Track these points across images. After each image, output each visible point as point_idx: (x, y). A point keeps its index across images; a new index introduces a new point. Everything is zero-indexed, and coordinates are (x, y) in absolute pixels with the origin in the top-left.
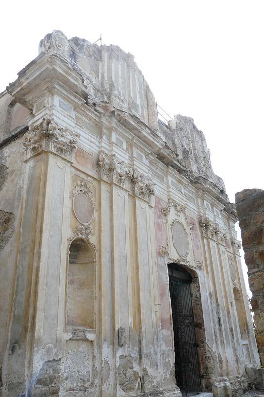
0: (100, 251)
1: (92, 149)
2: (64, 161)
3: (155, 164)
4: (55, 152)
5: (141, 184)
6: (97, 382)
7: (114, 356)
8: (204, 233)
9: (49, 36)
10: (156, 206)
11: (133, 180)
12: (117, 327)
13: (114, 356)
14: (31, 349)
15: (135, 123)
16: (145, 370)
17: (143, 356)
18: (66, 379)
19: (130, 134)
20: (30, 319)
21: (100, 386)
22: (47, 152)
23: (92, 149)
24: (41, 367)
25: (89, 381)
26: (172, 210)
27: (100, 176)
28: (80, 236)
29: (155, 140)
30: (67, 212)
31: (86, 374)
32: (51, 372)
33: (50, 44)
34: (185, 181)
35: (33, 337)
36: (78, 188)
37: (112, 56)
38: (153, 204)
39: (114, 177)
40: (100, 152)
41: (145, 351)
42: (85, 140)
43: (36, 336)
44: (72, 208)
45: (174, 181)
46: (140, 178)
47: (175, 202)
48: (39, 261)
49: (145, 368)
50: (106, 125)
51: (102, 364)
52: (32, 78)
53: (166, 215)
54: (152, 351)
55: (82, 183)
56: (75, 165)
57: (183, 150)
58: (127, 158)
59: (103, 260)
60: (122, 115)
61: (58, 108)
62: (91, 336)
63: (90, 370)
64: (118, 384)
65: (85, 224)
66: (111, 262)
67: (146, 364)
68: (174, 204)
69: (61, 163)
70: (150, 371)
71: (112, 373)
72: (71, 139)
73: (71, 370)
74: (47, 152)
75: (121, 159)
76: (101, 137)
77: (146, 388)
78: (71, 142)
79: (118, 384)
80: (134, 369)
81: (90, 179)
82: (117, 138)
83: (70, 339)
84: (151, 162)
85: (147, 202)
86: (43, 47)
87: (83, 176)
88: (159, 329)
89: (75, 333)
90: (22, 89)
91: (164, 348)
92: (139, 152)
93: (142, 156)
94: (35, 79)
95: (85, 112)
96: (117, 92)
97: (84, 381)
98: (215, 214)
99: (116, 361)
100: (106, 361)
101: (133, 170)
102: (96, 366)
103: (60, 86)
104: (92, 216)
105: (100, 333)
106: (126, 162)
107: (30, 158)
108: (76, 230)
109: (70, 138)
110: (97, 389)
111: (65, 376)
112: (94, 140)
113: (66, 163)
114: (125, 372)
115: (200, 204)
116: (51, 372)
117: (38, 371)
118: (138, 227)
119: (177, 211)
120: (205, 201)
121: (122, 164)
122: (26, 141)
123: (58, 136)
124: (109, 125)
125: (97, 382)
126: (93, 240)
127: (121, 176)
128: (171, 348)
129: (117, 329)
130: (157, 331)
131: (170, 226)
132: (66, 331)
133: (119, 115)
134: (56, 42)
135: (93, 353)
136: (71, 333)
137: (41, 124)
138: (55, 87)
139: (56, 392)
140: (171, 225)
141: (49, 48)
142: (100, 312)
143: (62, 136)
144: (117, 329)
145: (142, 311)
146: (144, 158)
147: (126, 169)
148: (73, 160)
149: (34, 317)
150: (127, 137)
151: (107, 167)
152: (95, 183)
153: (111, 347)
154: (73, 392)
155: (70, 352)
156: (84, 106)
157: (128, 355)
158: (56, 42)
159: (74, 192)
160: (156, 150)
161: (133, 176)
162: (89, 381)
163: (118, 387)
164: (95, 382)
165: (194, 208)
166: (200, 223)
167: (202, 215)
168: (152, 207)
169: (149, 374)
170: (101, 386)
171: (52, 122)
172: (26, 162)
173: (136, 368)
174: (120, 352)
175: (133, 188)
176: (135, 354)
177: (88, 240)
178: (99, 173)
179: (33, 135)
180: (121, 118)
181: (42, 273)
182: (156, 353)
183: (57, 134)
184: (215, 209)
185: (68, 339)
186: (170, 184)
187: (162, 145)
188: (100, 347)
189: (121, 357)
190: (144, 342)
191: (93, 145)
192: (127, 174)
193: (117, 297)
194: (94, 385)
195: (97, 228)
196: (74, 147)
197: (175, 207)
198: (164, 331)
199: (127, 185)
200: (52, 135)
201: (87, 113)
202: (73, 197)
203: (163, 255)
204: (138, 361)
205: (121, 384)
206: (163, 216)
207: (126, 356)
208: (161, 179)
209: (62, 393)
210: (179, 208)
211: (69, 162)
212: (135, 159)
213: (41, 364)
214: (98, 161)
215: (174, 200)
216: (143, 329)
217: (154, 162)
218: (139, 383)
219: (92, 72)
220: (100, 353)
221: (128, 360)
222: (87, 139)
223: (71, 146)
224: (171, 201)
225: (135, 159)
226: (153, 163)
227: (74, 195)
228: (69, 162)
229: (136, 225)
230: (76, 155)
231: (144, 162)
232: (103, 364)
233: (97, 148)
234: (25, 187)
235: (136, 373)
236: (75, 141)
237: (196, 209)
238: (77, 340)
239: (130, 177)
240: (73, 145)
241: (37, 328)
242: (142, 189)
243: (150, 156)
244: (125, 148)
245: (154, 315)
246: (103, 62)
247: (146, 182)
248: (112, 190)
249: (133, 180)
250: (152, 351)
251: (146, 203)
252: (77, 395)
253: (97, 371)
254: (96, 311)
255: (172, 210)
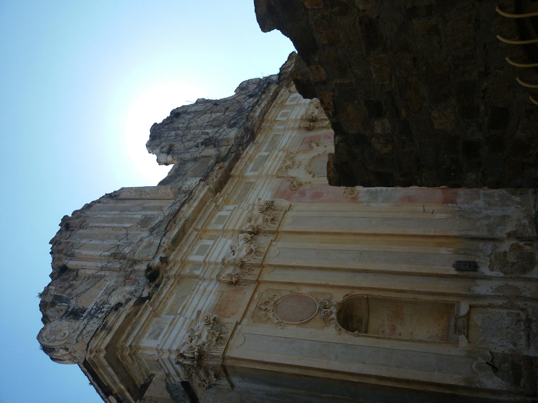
0: (353, 288)
1: (214, 291)
2: (235, 334)
3: (228, 195)
4: (224, 347)
5: (260, 221)
6: (520, 304)
7: (490, 278)
8: (323, 125)
9: (47, 349)
10: (288, 199)
11: (255, 233)
12: (453, 271)
13: (490, 278)
14: (478, 390)
15: (175, 227)
16: (510, 235)
17: (491, 236)
18: (515, 344)
19: (191, 234)
20: (441, 390)
21: (526, 300)
22: (224, 358)
23: (214, 291)
24: (500, 379)
25: (519, 314)
26: (292, 173)
27: (251, 282)
28: (334, 316)
29: (197, 197)
30: (303, 332)
31: (510, 318)
32: (506, 365)
33: (61, 348)
34: (250, 150)
35: (463, 388)
36: (270, 315)
37: (69, 253)
38: (285, 203)
39: (253, 262)
40: (219, 280)
41: (485, 233)
42: (202, 302)
43: (462, 384)
44: (298, 325)
45: (251, 166)
46: (253, 223)
47: (282, 168)
48: (369, 376)
49: (506, 234)
50: (179, 269)
51: (499, 296)
52: (116, 378)
53: (300, 184)
54: (485, 222)
55: (263, 308)
56: (238, 317)
57: (204, 146)
58: (224, 240)
59: (364, 284)
60: (165, 246)
61: (159, 341)
62: (464, 309)
63: (505, 311)
64: (525, 276)
65: (318, 307)
66: (367, 273)
67: (500, 233)
68: (284, 169)
69: (236, 341)
70: (510, 228)
71: (510, 283)
72: (203, 323)
73: (504, 338)
74: (224, 358)
75: (227, 248)
76: (197, 277)
77: (532, 235)
78: (208, 323)
79: (525, 276)
80: (508, 250)
81: (256, 297)
82: (197, 254)
83: (467, 337)
84: (227, 202)
85: (284, 214)
86: (65, 358)
87: (253, 307)
88: (456, 209)
89: (459, 330)
90: (128, 390)
91: (480, 203)
92: (214, 221)
93: (220, 216)
94: (117, 374)
95: (162, 300)
96: (126, 249)
97: (519, 321)
98: (294, 103)
99: (496, 277)
100: (495, 290)
101: (242, 232)
102: (501, 303)
103: (127, 338)
104: (306, 297)
105: (459, 295)
106: (230, 242)
107: (229, 381)
108: (326, 320)
109: (201, 324)
110: (529, 304)
111: (511, 346)
112: (202, 288)
113: (237, 331)
114: (510, 265)
115: (282, 127)
116: (506, 365)
117: (504, 382)
118: (319, 230)
119: (293, 165)
120: (278, 119)
121: (234, 249)
122: (204, 386)
123: (200, 343)
124: (179, 265)
125: (520, 304)
126: (339, 297)
127: (252, 251)
128: (482, 191)
129: (456, 273)
130: (459, 211)
131: (316, 178)
132: (456, 343)
133: (165, 251)
134: (59, 340)
135: (485, 307)
136: (460, 337)
137: (183, 365)
138: (130, 346)
139: (530, 360)
140: (313, 176)
141: (67, 349)
142: (433, 294)
143: (200, 337)
144: (456, 273)
145: (432, 233)
146: (222, 213)
147: (241, 243)
148: (233, 320)
149: (439, 385)
150: (195, 238)
151: (238, 270)
152: (262, 288)
153: (478, 282)
154: (531, 337)
155: (482, 338)
156: (154, 301)
157: (489, 259)
158: (59, 340)
159: (276, 321)
160: (210, 194)
161: (250, 233)
162: (519, 314)
163: (528, 275)
164: (521, 306)
165: (287, 138)
166: (309, 129)
167: (297, 125)
168: (291, 206)
169: (515, 229)
170: (526, 299)
171: (182, 351)
172: (232, 386)
173: (505, 247)
174: (485, 270)
175: (266, 233)
176: (489, 247)
177: (339, 304)
178: (248, 282)
179: (197, 377)
180: (169, 249)
181: (384, 373)
182: (488, 217)
183: (198, 344)
184: (288, 103)
185: (466, 340)
186: (257, 173)
187: (204, 186)
188: (478, 297)
189: (492, 269)
190: (473, 233)
191: (209, 288)
192: (247, 241)
193: (413, 269)
194: (524, 307)
195: (322, 290)
196: (214, 319)
197: (288, 167)
198: (458, 200)
199: (263, 241)
200: (199, 351)
201: (164, 298)
202: (282, 322)
203: (356, 193)
204: (497, 244)
205: (525, 271)
206: (302, 188)
207: (490, 261)
208: (250, 186)
209: (532, 352)
210: (289, 163)
211: (235, 328)
212: (225, 228)
213: (497, 379)
214: (231, 283)
215: (279, 170)
216: (455, 233)
217: (226, 196)
218: (525, 244)
219: (98, 285)
220: (485, 297)
221: (496, 258)
222: (200, 299)
223: (213, 324)
224: (280, 174)
225: (225, 228)
226: (227, 199)
227: (280, 321)
228: (235, 328)
229: (317, 233)
230: (224, 317)
231: (228, 213)
232: (499, 294)
233: (213, 284)
234: (268, 388)
235: (513, 248)
236: (206, 318)
237: (289, 134)
238: (468, 327)
239: (252, 237)
240: (212, 322)
241: (453, 383)
242: (267, 220)
243: (218, 203)
244: (210, 243)
245: (438, 216)
246: (79, 267)
247: (256, 212)
248: (270, 265)
249: (255, 233)
250: (485, 222)
251: (286, 215)
252: (535, 331)
253: (507, 302)
254: (434, 298)
255: (292, 173)
